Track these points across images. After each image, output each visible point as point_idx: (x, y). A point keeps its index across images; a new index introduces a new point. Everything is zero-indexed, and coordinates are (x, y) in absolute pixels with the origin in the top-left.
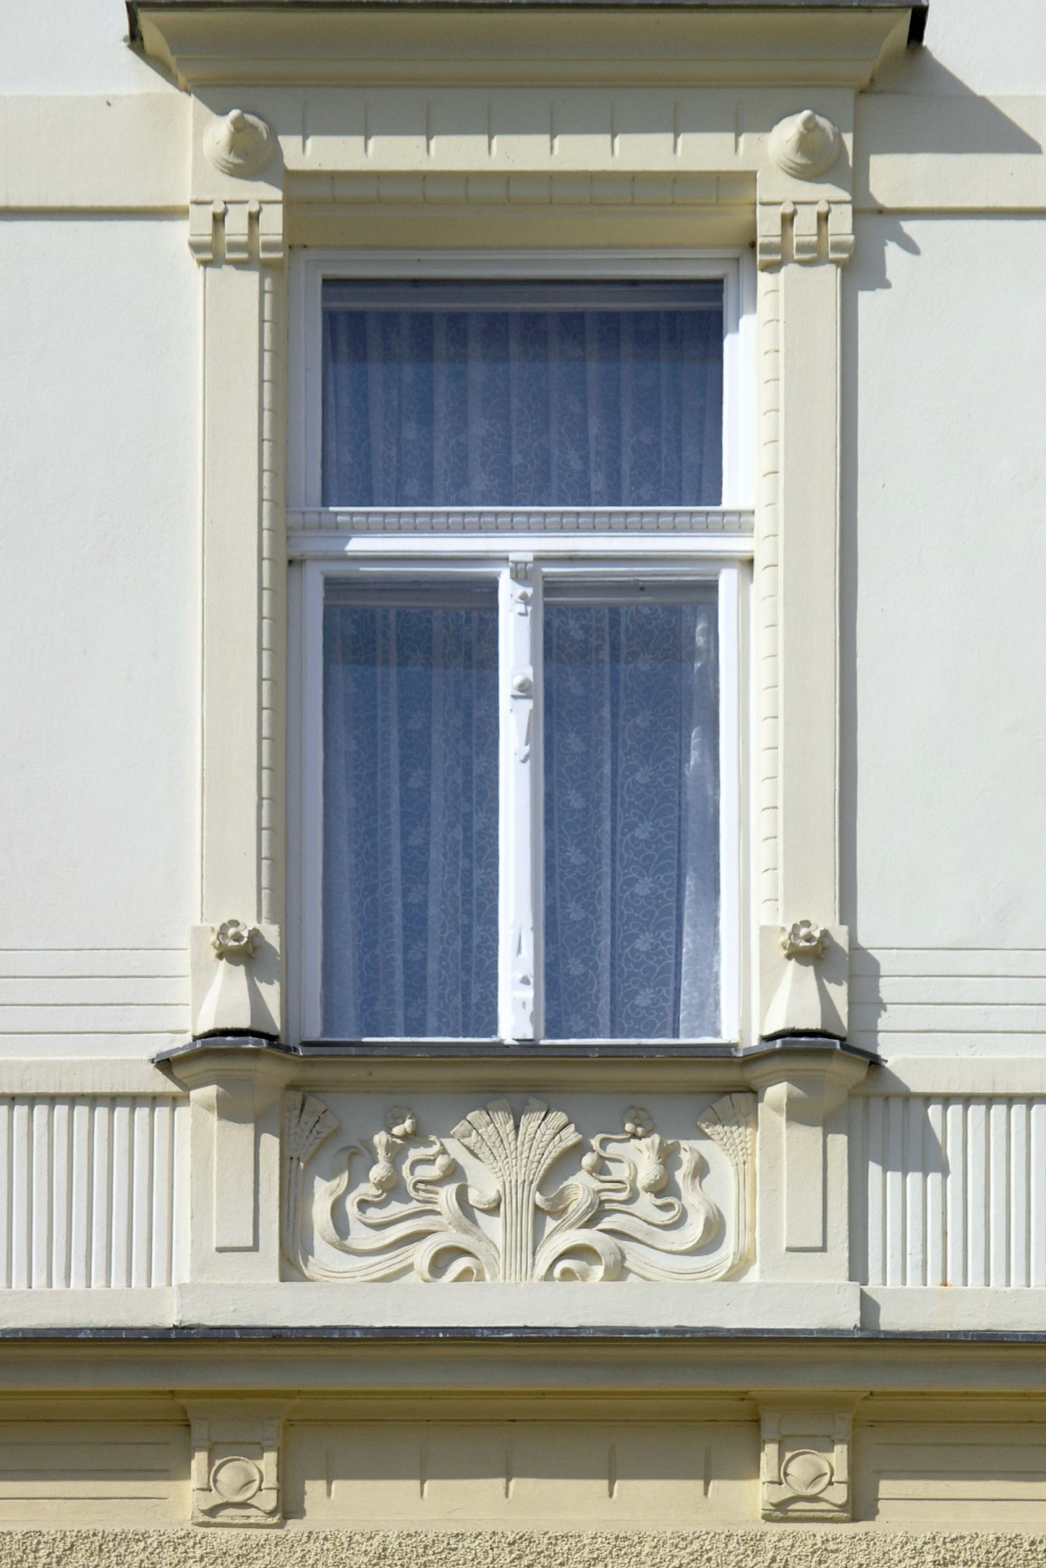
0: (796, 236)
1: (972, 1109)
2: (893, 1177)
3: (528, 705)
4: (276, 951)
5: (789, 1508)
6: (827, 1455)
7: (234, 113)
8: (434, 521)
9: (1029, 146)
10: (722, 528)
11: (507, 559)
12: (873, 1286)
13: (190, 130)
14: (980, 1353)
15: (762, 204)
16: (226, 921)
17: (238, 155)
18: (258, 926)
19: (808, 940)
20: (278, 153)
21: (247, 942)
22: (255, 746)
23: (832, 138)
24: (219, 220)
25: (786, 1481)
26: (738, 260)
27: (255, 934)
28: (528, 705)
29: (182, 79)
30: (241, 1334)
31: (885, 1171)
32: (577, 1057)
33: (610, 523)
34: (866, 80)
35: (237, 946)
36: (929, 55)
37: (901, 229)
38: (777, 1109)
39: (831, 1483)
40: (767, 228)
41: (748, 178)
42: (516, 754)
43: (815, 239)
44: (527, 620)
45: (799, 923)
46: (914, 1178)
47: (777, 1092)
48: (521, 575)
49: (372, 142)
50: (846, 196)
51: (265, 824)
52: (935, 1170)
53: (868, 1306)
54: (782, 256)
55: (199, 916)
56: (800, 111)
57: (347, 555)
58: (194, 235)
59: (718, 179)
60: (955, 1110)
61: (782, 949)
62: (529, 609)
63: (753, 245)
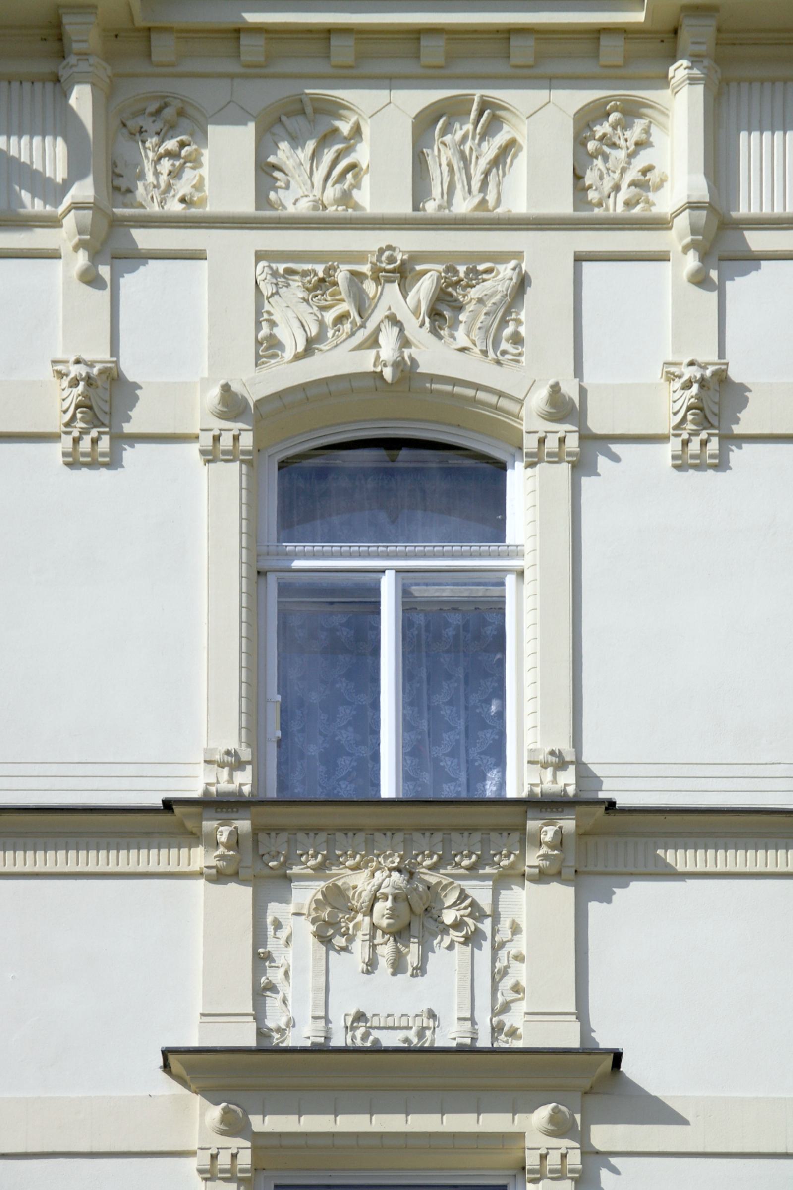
7: (224, 1105)
9: (684, 1122)
10: (508, 555)
13: (198, 1112)
15: (529, 1149)
17: (225, 1125)
20: (248, 1123)
23: (568, 1116)
24: (214, 1157)
26: (515, 1175)
29: (193, 1087)
34: (588, 1088)
36: (625, 1075)
37: (609, 1161)
40: (532, 1160)
41: (521, 1136)
43: (560, 1166)
49: (303, 1118)
50: (578, 1146)
63: (524, 1168)
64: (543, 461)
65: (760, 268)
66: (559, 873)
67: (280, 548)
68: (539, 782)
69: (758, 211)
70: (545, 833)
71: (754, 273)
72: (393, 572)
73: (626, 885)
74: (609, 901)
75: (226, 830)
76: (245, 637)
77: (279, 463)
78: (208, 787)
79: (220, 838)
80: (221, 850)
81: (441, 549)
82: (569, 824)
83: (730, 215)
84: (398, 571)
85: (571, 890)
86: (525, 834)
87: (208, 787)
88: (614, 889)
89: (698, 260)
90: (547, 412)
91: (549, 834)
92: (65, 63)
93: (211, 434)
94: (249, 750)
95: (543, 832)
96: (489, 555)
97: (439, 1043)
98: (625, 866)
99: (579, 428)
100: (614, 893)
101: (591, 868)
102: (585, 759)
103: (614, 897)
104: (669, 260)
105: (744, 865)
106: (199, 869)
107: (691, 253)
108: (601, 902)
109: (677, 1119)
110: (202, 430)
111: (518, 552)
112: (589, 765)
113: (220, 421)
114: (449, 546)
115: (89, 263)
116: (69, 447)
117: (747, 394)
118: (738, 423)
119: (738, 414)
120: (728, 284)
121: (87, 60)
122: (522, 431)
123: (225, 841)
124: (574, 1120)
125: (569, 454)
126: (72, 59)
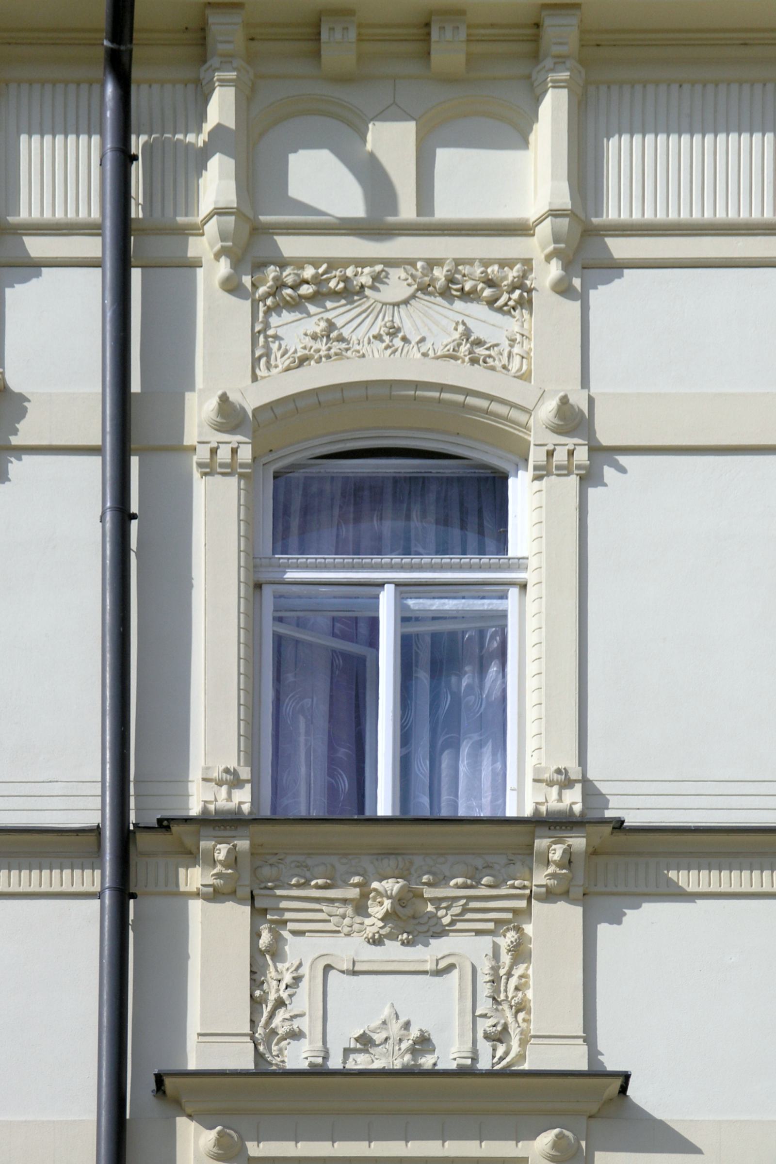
7: (219, 1128)
10: (509, 568)
17: (557, 1150)
20: (244, 1149)
22: (237, 586)
23: (573, 1141)
36: (631, 1100)
51: (242, 687)
58: (200, 459)
64: (552, 474)
65: (41, 275)
66: (234, 893)
67: (273, 560)
68: (544, 801)
69: (724, 215)
70: (553, 852)
71: (34, 281)
72: (392, 586)
73: (637, 907)
74: (619, 922)
75: (223, 848)
77: (274, 472)
78: (538, 806)
79: (218, 856)
80: (219, 869)
81: (458, 560)
82: (578, 842)
83: (6, 219)
84: (398, 585)
85: (579, 910)
86: (533, 853)
87: (538, 806)
88: (626, 911)
89: (560, 268)
90: (555, 424)
91: (557, 853)
92: (540, 67)
93: (208, 447)
94: (249, 769)
95: (217, 850)
96: (489, 568)
97: (290, 1065)
98: (606, 886)
100: (625, 914)
101: (600, 888)
102: (590, 776)
103: (625, 919)
104: (201, 266)
105: (18, 885)
106: (196, 890)
107: (554, 262)
108: (611, 923)
110: (199, 443)
111: (519, 565)
112: (596, 783)
113: (553, 434)
114: (359, 558)
115: (232, 271)
116: (247, 458)
117: (26, 404)
118: (16, 434)
119: (17, 425)
120: (592, 293)
121: (564, 62)
122: (529, 442)
123: (223, 859)
124: (580, 1146)
125: (579, 467)
126: (214, 61)
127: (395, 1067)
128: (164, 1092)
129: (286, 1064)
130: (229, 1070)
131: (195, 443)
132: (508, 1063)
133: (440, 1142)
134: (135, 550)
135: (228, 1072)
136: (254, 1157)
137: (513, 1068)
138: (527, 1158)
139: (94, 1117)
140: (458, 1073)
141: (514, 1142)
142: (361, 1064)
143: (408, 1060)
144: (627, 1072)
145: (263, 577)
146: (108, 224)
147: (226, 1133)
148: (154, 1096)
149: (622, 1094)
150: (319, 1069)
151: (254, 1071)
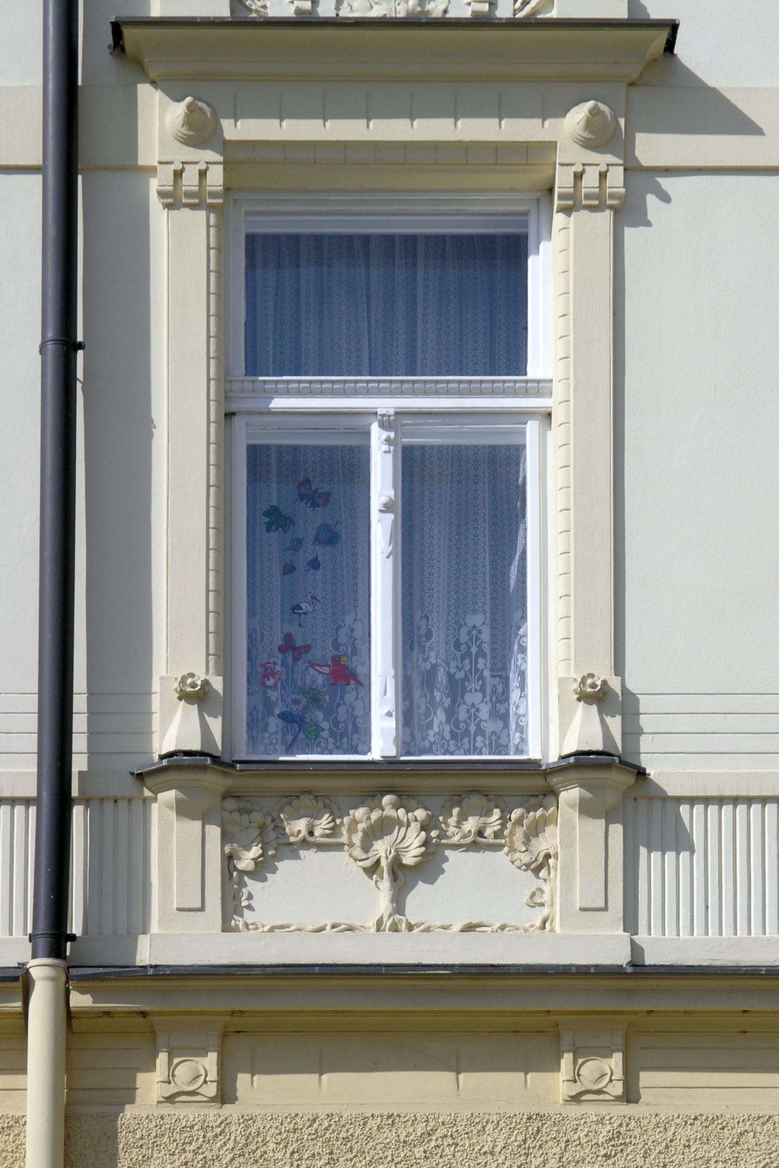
0: (584, 188)
1: (724, 808)
2: (655, 856)
3: (391, 516)
4: (219, 693)
5: (582, 1098)
6: (608, 1060)
7: (188, 99)
8: (289, 387)
11: (376, 413)
12: (641, 938)
14: (559, 982)
15: (561, 165)
16: (185, 673)
18: (207, 678)
19: (193, 687)
20: (219, 129)
21: (200, 689)
23: (609, 118)
24: (178, 175)
25: (173, 1080)
27: (206, 683)
28: (391, 516)
30: (594, 970)
31: (649, 852)
32: (515, 770)
33: (311, 389)
35: (192, 691)
38: (571, 806)
39: (205, 1082)
40: (563, 181)
41: (551, 146)
42: (382, 553)
44: (390, 457)
45: (586, 675)
46: (670, 856)
47: (570, 795)
48: (386, 424)
50: (621, 162)
52: (686, 850)
53: (636, 949)
54: (574, 202)
55: (165, 669)
56: (588, 101)
57: (270, 411)
59: (528, 148)
60: (698, 809)
61: (574, 694)
62: (392, 448)
63: (551, 190)
76: (213, 549)
99: (624, 161)
109: (747, 127)
110: (160, 163)
111: (539, 389)
124: (617, 124)
127: (399, 15)
128: (123, 49)
129: (268, 11)
130: (201, 18)
131: (156, 164)
132: (532, 9)
133: (452, 120)
134: (82, 380)
135: (199, 20)
136: (231, 141)
137: (539, 16)
138: (556, 143)
139: (40, 84)
140: (473, 23)
141: (540, 120)
142: (357, 10)
143: (414, 5)
144: (674, 20)
145: (234, 408)
146: (45, 795)
147: (197, 106)
148: (111, 53)
149: (668, 53)
150: (306, 18)
151: (230, 20)
